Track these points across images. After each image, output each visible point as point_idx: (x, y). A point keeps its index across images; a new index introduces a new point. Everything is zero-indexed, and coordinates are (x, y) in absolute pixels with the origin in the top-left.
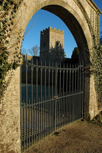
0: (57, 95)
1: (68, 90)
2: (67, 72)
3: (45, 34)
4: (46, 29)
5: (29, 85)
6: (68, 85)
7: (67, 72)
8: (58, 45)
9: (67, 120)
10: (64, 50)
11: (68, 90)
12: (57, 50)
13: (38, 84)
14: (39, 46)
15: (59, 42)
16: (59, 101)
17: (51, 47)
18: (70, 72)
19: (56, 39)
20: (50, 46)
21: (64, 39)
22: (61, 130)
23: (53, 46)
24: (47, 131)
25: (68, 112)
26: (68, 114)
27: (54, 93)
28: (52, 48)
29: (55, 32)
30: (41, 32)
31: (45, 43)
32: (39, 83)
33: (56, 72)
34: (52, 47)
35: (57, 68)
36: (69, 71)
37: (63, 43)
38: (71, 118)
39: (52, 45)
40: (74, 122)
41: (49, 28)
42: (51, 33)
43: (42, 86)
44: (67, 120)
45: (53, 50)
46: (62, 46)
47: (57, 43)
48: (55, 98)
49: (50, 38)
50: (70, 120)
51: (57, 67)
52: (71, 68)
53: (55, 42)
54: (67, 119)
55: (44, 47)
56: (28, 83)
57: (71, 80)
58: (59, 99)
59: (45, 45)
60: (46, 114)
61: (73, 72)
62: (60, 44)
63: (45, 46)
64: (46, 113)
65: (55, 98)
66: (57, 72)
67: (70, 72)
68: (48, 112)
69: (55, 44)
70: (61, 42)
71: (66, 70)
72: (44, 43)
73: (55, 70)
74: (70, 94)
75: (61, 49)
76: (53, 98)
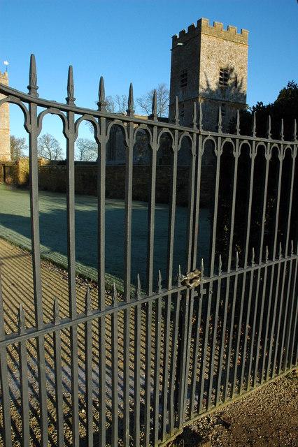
0: (199, 267)
1: (255, 243)
2: (253, 155)
3: (185, 44)
4: (191, 28)
5: (117, 205)
6: (257, 216)
7: (253, 155)
8: (227, 80)
9: (241, 360)
10: (245, 97)
11: (255, 243)
12: (224, 97)
13: (157, 202)
14: (168, 88)
15: (232, 70)
16: (206, 297)
17: (205, 87)
18: (268, 156)
19: (220, 62)
20: (200, 83)
21: (249, 61)
22: (209, 420)
23: (211, 84)
24: (148, 425)
25: (251, 324)
26: (250, 334)
27: (181, 258)
28: (208, 89)
29: (219, 37)
30: (174, 38)
31: (186, 74)
32: (163, 199)
33: (194, 153)
34: (208, 85)
35: (203, 132)
36: (261, 150)
37: (242, 73)
38: (262, 351)
39: (207, 82)
40: (273, 381)
41: (199, 22)
42: (207, 41)
43: (177, 212)
44: (241, 360)
45: (211, 97)
46: (239, 84)
47: (225, 74)
48: (184, 283)
49: (202, 57)
50: (254, 362)
51: (198, 126)
52: (273, 137)
53: (218, 72)
54: (242, 356)
55: (182, 86)
56: (108, 196)
57: (272, 193)
58: (206, 286)
59: (186, 80)
60: (165, 323)
61: (281, 157)
62: (233, 76)
63: (186, 85)
64: (165, 316)
65: (184, 283)
66: (201, 151)
67: (268, 156)
68: (173, 314)
69: (219, 76)
70: (237, 70)
71: (245, 145)
72: (183, 76)
73: (187, 142)
74: (264, 260)
75: (237, 93)
76: (175, 283)
